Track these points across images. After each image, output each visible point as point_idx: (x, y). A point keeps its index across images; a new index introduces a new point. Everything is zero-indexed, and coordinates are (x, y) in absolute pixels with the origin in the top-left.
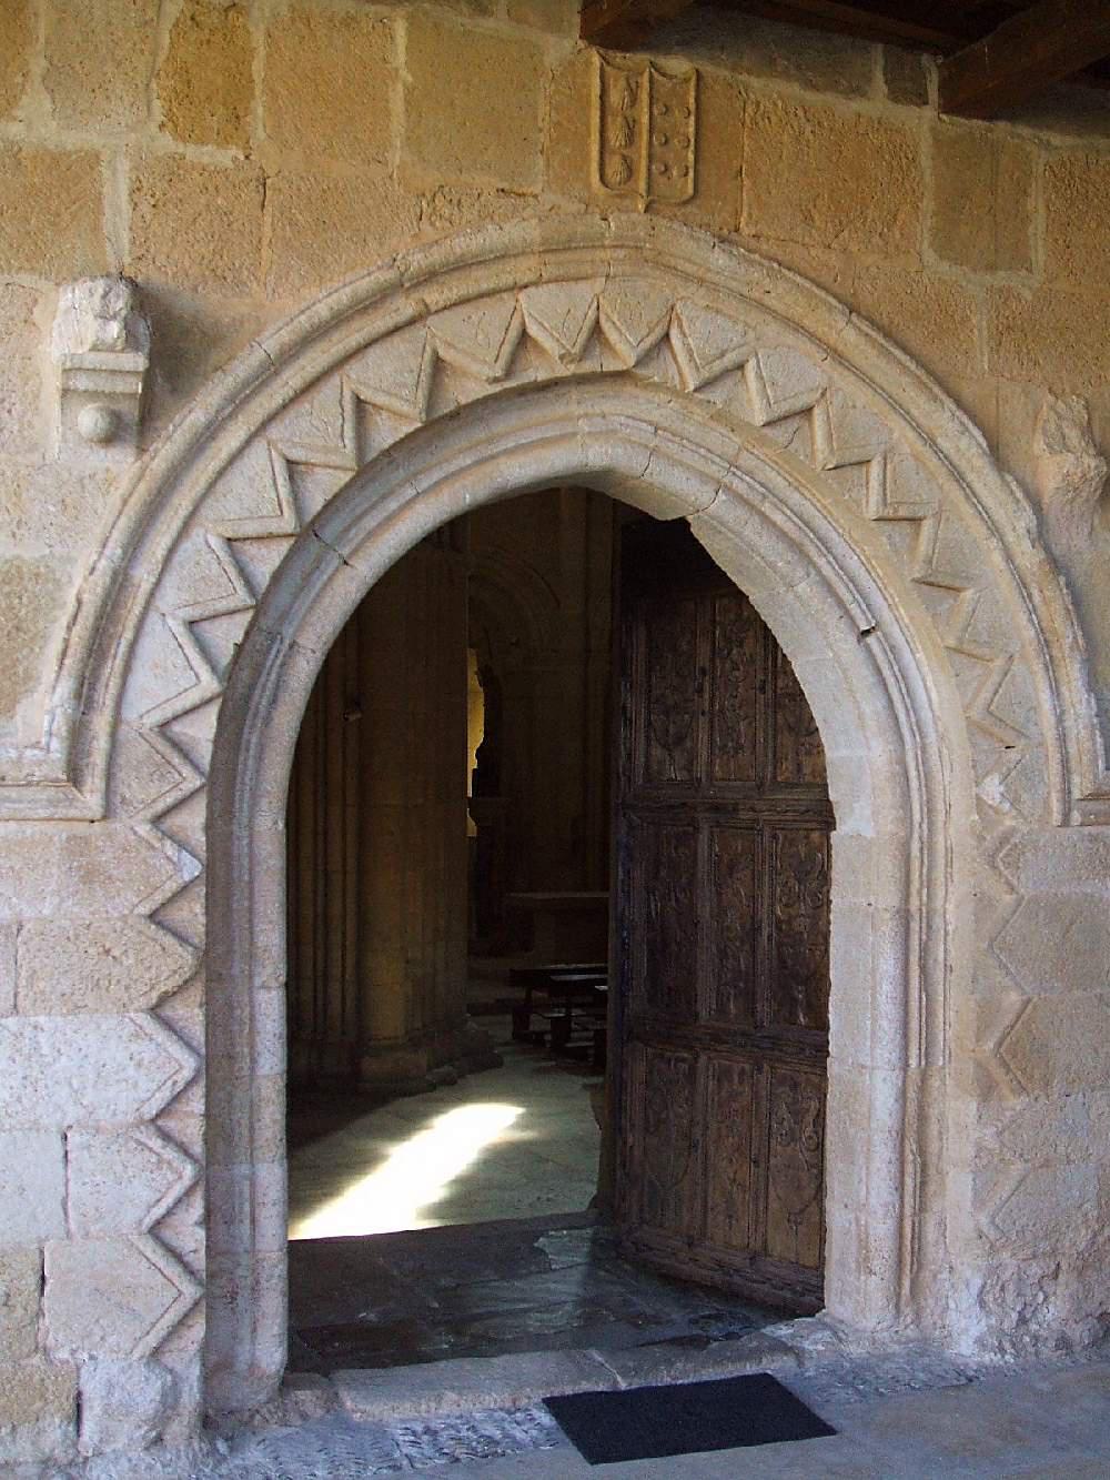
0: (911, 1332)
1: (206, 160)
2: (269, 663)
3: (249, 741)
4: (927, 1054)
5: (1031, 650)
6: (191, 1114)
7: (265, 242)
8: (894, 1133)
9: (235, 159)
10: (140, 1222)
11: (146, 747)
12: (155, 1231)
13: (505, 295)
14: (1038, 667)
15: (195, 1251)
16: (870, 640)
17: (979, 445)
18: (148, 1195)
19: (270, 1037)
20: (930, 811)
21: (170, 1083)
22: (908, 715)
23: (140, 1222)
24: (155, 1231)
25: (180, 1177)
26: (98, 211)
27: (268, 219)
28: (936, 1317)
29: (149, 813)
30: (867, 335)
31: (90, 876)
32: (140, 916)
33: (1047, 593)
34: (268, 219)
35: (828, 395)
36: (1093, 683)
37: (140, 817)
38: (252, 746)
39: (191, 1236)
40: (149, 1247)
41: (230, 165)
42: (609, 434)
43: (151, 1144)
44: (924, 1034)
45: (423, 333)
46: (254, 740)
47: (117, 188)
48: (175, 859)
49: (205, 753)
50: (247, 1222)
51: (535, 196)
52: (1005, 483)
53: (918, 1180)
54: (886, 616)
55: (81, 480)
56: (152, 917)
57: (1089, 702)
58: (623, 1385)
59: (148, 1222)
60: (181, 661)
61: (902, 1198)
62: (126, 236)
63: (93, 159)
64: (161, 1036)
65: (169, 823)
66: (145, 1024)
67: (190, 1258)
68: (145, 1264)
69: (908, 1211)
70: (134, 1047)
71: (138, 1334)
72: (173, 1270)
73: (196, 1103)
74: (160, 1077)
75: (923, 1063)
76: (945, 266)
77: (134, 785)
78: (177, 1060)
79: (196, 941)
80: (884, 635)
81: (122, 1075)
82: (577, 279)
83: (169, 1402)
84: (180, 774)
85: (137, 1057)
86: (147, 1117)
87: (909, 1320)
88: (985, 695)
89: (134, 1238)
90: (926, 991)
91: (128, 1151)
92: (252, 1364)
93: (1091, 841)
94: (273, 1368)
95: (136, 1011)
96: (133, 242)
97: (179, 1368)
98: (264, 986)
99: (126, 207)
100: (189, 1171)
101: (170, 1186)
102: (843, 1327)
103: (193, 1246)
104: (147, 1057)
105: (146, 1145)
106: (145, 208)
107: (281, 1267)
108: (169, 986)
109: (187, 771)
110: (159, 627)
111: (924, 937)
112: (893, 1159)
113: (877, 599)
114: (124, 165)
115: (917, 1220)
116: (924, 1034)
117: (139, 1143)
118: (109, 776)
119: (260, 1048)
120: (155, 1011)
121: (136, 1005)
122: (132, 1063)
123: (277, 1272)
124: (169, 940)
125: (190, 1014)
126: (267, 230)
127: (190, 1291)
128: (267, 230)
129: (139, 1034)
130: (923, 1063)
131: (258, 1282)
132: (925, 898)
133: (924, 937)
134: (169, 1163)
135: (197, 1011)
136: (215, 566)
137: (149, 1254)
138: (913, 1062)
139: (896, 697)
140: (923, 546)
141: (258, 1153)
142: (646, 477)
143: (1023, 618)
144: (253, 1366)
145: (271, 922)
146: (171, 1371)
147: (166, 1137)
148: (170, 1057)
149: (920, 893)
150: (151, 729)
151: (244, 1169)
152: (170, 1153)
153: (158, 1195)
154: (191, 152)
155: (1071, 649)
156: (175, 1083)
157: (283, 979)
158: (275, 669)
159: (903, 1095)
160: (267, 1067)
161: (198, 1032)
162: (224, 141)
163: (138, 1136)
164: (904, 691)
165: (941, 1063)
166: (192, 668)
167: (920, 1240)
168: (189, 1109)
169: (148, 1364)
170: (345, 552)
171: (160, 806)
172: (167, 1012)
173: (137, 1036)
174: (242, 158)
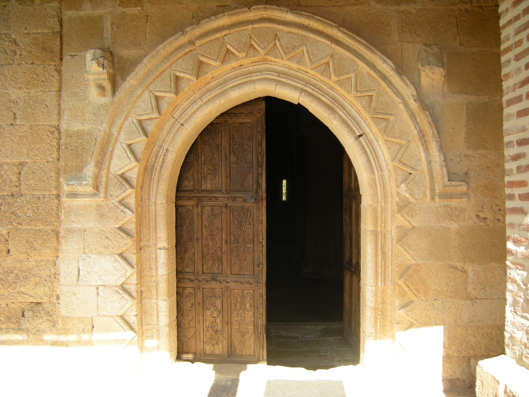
1: (131, 12)
2: (159, 155)
5: (417, 138)
7: (147, 33)
9: (139, 11)
11: (116, 180)
14: (420, 144)
16: (361, 138)
17: (391, 67)
20: (385, 197)
26: (103, 32)
27: (148, 26)
31: (102, 216)
33: (421, 117)
34: (148, 26)
36: (441, 149)
41: (137, 12)
43: (120, 291)
47: (107, 25)
50: (155, 316)
51: (229, 6)
52: (404, 80)
54: (367, 130)
55: (99, 106)
57: (440, 156)
62: (110, 37)
63: (101, 17)
67: (132, 325)
68: (119, 325)
76: (378, 6)
81: (111, 272)
88: (399, 155)
93: (444, 207)
96: (112, 39)
99: (110, 29)
106: (115, 29)
110: (120, 146)
113: (363, 125)
114: (109, 17)
118: (106, 188)
119: (159, 267)
126: (148, 29)
128: (148, 29)
129: (116, 261)
132: (383, 227)
136: (134, 128)
143: (413, 127)
148: (124, 267)
149: (381, 226)
151: (154, 301)
154: (127, 10)
155: (432, 137)
158: (162, 157)
162: (135, 6)
170: (182, 122)
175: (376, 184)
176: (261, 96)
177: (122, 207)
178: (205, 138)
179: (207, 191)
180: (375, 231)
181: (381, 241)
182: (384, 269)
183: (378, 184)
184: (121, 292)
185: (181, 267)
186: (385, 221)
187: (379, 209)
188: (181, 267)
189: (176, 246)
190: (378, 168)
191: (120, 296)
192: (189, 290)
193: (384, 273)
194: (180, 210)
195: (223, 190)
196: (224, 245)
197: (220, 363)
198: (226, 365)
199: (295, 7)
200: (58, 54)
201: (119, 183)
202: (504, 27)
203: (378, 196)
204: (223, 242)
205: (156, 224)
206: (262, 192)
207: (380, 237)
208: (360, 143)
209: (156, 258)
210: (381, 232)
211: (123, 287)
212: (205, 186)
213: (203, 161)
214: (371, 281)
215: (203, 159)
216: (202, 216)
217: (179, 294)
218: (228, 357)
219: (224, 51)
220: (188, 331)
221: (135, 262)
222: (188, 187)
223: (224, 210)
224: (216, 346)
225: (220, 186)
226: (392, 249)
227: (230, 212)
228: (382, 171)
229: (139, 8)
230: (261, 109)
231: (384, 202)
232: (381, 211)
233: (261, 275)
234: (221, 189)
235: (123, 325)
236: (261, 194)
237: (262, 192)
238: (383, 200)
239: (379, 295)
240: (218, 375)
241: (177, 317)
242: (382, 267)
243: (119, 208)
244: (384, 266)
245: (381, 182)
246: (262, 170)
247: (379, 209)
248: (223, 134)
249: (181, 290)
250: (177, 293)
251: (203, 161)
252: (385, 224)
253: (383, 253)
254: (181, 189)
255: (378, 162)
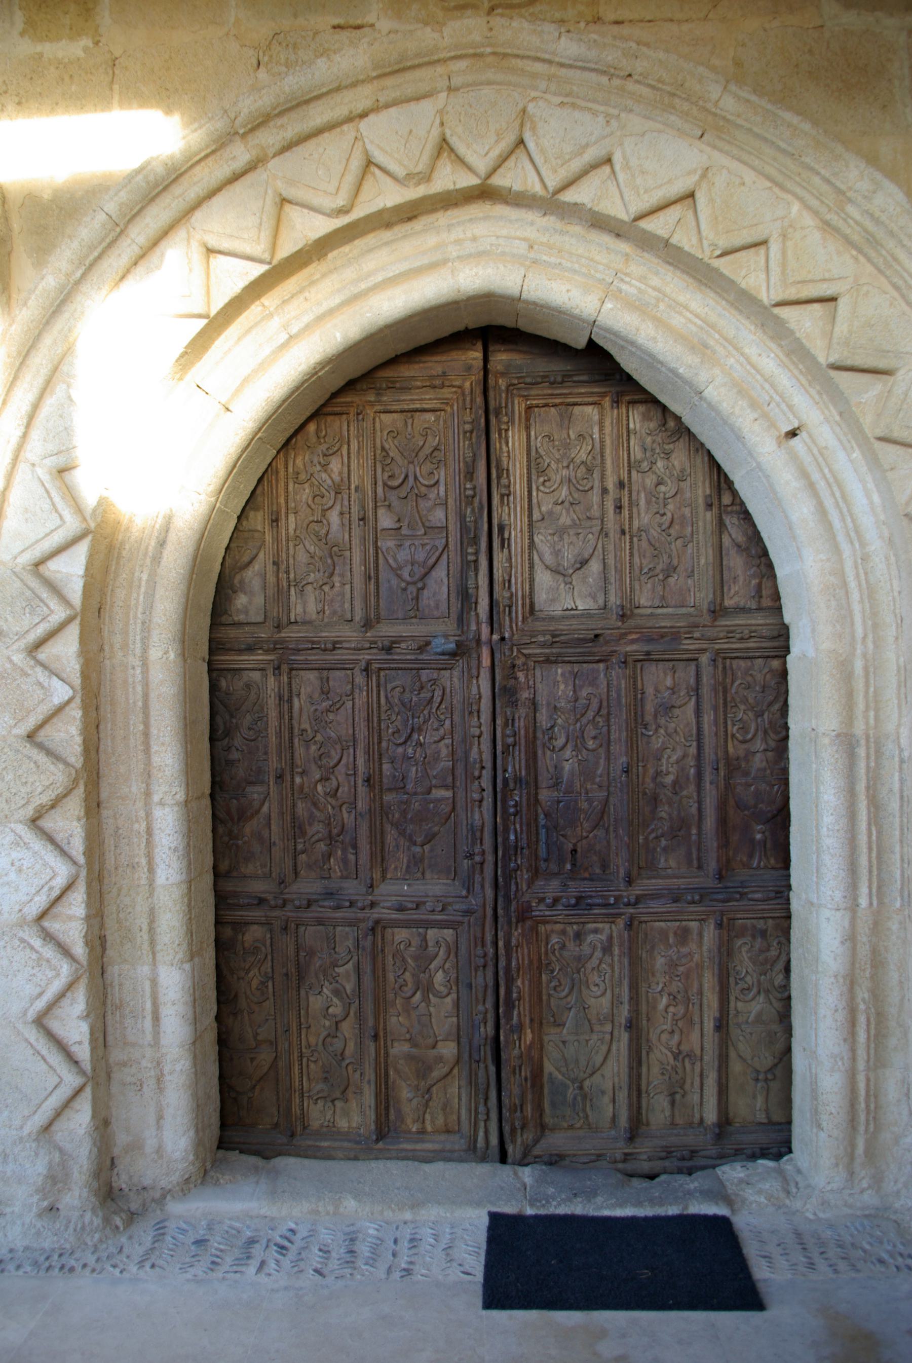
0: (869, 1199)
3: (140, 579)
4: (880, 891)
6: (71, 918)
8: (841, 980)
9: (86, 49)
10: (25, 1013)
11: (18, 584)
12: (40, 1022)
13: (345, 127)
15: (80, 1043)
18: (30, 990)
19: (166, 850)
21: (46, 889)
22: (843, 520)
23: (25, 1013)
24: (40, 1022)
25: (58, 975)
28: (900, 1185)
29: (22, 644)
30: (748, 101)
32: (16, 736)
35: (710, 175)
37: (15, 647)
38: (143, 583)
39: (75, 1029)
40: (32, 1034)
42: (480, 255)
43: (32, 942)
44: (875, 873)
45: (265, 176)
46: (145, 577)
48: (46, 684)
49: (75, 591)
51: (372, 25)
53: (873, 1032)
56: (30, 736)
58: (529, 1211)
59: (32, 1014)
60: (47, 506)
61: (853, 1050)
64: (37, 844)
65: (42, 655)
66: (23, 833)
67: (74, 1049)
69: (861, 1065)
70: (15, 855)
71: (26, 1113)
72: (56, 1059)
73: (76, 905)
74: (38, 882)
75: (875, 903)
77: (10, 619)
78: (51, 868)
79: (72, 760)
80: (810, 436)
82: (418, 99)
83: (56, 1179)
84: (48, 607)
85: (17, 864)
86: (29, 918)
87: (865, 1184)
89: (20, 1026)
90: (876, 825)
91: (13, 948)
92: (160, 1147)
94: (178, 1155)
95: (16, 822)
97: (68, 1147)
98: (161, 803)
100: (65, 969)
101: (49, 982)
102: (799, 1178)
103: (77, 1038)
104: (26, 864)
105: (29, 944)
107: (183, 1062)
108: (45, 799)
109: (53, 603)
111: (873, 764)
112: (840, 1007)
115: (872, 1076)
116: (875, 873)
117: (22, 941)
119: (157, 860)
120: (34, 822)
121: (16, 817)
122: (13, 869)
123: (178, 1067)
124: (41, 758)
125: (69, 825)
127: (72, 1080)
129: (18, 843)
130: (875, 903)
131: (162, 1075)
132: (872, 722)
133: (873, 764)
134: (48, 961)
135: (75, 823)
137: (32, 1040)
138: (863, 902)
139: (829, 503)
140: (841, 328)
141: (159, 956)
142: (524, 296)
144: (159, 1150)
145: (163, 744)
146: (61, 1150)
147: (48, 937)
150: (24, 568)
151: (144, 970)
152: (49, 952)
153: (38, 990)
156: (51, 889)
157: (181, 796)
159: (851, 938)
160: (164, 878)
161: (77, 847)
163: (21, 934)
164: (838, 494)
165: (898, 904)
166: (57, 511)
167: (876, 1097)
168: (70, 912)
169: (37, 1140)
171: (32, 637)
172: (47, 823)
173: (18, 844)
174: (91, 45)
175: (845, 584)
176: (471, 326)
177: (39, 672)
178: (299, 462)
179: (304, 623)
180: (846, 735)
181: (868, 766)
182: (879, 857)
183: (853, 584)
184: (37, 943)
185: (227, 862)
186: (876, 702)
187: (859, 665)
188: (227, 862)
189: (212, 796)
190: (852, 534)
191: (34, 956)
192: (253, 934)
193: (879, 869)
194: (223, 684)
195: (357, 618)
196: (362, 790)
197: (356, 1159)
198: (374, 1164)
199: (582, 25)
200: (153, 695)
201: (28, 593)
202: (70, 986)
203: (852, 624)
204: (360, 782)
205: (147, 724)
206: (478, 624)
207: (861, 752)
208: (794, 457)
209: (149, 832)
210: (868, 740)
211: (43, 929)
212: (299, 609)
213: (291, 531)
214: (838, 895)
215: (292, 526)
216: (290, 701)
217: (222, 946)
218: (377, 1141)
219: (356, 163)
220: (252, 1060)
221: (81, 849)
222: (247, 613)
223: (360, 679)
224: (339, 1104)
225: (347, 606)
226: (901, 791)
227: (378, 686)
228: (863, 545)
229: (86, 42)
230: (469, 368)
231: (874, 642)
232: (866, 669)
233: (478, 878)
234: (349, 617)
235: (44, 1052)
236: (473, 627)
237: (478, 624)
238: (870, 636)
239: (865, 939)
240: (174, 564)
241: (218, 1018)
242: (870, 849)
243: (27, 675)
244: (878, 847)
245: (863, 577)
246: (476, 553)
247: (859, 665)
248: (354, 445)
249: (228, 932)
250: (217, 941)
251: (291, 531)
252: (877, 710)
253: (875, 804)
254: (224, 619)
255: (851, 515)
